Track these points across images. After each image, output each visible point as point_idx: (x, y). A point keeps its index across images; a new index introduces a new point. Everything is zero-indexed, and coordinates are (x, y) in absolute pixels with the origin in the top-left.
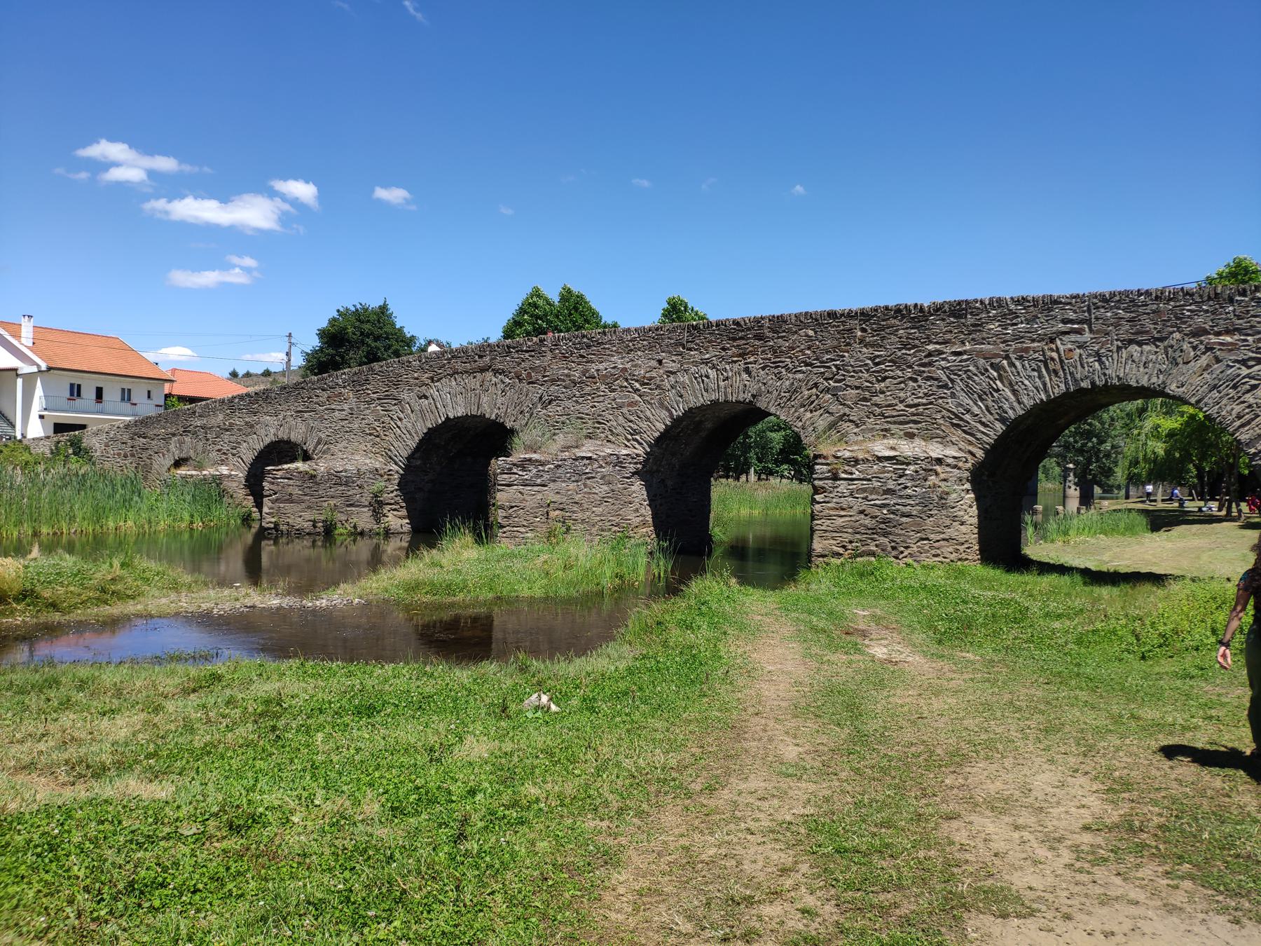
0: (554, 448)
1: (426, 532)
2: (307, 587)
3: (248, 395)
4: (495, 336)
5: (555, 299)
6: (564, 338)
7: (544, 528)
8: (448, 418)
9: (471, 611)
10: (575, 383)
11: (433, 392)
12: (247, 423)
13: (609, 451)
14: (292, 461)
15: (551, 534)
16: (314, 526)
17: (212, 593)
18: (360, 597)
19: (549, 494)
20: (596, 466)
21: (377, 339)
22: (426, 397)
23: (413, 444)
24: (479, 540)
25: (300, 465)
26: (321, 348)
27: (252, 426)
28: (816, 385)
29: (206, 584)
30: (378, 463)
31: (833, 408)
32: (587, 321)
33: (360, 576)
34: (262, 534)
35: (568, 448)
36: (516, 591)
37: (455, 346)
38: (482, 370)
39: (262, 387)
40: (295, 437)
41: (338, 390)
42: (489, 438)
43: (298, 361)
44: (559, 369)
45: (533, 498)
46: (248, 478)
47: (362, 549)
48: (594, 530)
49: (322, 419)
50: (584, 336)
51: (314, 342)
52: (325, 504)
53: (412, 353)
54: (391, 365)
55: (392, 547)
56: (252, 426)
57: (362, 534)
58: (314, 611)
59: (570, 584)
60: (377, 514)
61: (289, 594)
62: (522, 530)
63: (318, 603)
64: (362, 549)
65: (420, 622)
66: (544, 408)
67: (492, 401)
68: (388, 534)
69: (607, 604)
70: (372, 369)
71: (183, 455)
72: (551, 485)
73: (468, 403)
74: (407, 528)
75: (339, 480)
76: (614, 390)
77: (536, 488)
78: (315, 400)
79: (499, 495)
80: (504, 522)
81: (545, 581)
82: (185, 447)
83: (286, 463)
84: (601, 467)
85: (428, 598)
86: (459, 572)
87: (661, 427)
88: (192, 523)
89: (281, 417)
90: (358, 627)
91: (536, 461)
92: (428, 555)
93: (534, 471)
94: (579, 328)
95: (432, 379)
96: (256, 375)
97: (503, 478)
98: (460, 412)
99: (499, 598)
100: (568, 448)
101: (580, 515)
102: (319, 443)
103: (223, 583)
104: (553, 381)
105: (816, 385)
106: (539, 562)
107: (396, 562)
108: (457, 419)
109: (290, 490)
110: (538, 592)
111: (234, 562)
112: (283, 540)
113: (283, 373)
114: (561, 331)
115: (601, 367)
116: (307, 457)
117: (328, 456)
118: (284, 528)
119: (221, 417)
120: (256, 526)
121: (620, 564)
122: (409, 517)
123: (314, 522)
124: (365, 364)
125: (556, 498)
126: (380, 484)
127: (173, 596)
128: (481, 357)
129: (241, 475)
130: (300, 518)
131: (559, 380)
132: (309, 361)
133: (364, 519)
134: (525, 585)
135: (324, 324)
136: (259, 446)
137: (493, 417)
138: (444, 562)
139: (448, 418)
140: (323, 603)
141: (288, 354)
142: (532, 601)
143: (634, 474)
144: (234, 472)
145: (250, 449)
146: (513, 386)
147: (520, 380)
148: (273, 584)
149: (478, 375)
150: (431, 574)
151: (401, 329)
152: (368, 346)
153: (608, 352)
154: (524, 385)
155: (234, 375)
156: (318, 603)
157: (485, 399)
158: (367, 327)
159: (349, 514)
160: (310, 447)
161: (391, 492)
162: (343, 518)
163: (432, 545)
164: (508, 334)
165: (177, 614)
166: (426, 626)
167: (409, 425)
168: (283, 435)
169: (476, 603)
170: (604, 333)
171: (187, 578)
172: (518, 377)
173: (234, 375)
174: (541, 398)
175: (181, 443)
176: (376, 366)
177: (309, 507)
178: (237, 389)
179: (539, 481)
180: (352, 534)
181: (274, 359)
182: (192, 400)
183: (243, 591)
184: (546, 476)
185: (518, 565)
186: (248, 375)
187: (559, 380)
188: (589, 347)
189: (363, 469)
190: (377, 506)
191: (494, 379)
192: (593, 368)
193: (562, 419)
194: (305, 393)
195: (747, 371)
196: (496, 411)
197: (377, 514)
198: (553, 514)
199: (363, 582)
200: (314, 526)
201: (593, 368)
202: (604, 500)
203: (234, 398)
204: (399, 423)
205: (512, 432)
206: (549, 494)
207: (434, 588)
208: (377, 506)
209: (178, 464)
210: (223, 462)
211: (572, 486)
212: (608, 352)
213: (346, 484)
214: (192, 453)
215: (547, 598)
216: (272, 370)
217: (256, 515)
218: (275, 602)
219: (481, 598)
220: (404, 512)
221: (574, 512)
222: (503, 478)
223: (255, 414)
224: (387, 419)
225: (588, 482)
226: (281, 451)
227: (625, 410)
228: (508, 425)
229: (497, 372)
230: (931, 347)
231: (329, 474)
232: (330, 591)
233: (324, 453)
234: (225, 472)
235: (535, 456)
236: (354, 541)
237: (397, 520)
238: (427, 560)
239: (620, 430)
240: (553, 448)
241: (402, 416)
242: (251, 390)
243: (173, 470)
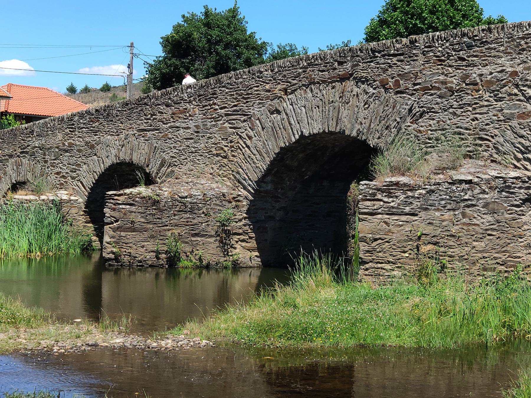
0: (425, 169)
1: (277, 267)
2: (148, 325)
3: (88, 112)
4: (357, 38)
5: (248, 33)
6: (440, 38)
7: (413, 266)
8: (302, 136)
9: (331, 360)
10: (452, 91)
11: (286, 105)
12: (87, 143)
13: (494, 173)
14: (134, 186)
15: (422, 273)
16: (158, 258)
17: (52, 329)
18: (208, 339)
19: (419, 225)
20: (477, 191)
21: (227, 46)
22: (278, 112)
23: (263, 166)
24: (338, 276)
25: (142, 190)
26: (165, 58)
27: (92, 147)
29: (45, 319)
30: (224, 187)
32: (464, 16)
33: (205, 313)
34: (103, 265)
35: (442, 170)
36: (381, 338)
37: (312, 51)
38: (343, 79)
39: (102, 104)
40: (137, 158)
41: (183, 106)
42: (350, 157)
43: (140, 73)
44: (433, 75)
45: (401, 228)
46: (88, 204)
47: (209, 282)
48: (475, 269)
49: (166, 138)
50: (464, 35)
51: (156, 52)
52: (169, 234)
53: (263, 62)
54: (239, 77)
55: (240, 283)
56: (92, 147)
57: (208, 267)
58: (157, 353)
59: (446, 332)
60: (225, 246)
61: (132, 332)
62: (388, 267)
63: (163, 343)
64: (209, 282)
65: (274, 369)
66: (415, 122)
67: (352, 114)
68: (237, 267)
69: (493, 357)
70: (219, 81)
71: (21, 179)
72: (422, 214)
73: (325, 118)
74: (257, 261)
75: (185, 206)
76: (500, 100)
77: (404, 218)
78: (158, 116)
79: (360, 226)
80: (366, 257)
81: (415, 329)
82: (22, 169)
83: (128, 187)
84: (484, 192)
85: (282, 343)
86: (316, 314)
88: (30, 251)
89: (122, 136)
90: (204, 372)
91: (405, 185)
92: (282, 293)
93: (402, 197)
94: (457, 25)
95: (285, 90)
96: (95, 91)
97: (366, 205)
98: (317, 128)
99: (362, 346)
100: (442, 170)
101: (457, 251)
102: (162, 165)
103: (64, 319)
104: (425, 89)
106: (407, 306)
107: (246, 301)
108: (313, 136)
109: (132, 217)
110: (408, 342)
111: (75, 295)
112: (125, 272)
113: (124, 89)
114: (436, 29)
115: (485, 71)
116: (149, 181)
117: (172, 180)
118: (126, 259)
119: (60, 136)
120: (96, 256)
121: (506, 310)
122: (259, 249)
123: (158, 253)
124: (213, 75)
125: (428, 230)
126: (228, 211)
127: (12, 331)
128: (340, 63)
129: (81, 200)
130: (143, 248)
131: (433, 88)
132: (152, 73)
133: (209, 250)
134: (392, 333)
135: (168, 31)
136: (100, 169)
137: (354, 134)
138: (299, 301)
139: (302, 136)
140: (168, 343)
141: (129, 66)
142: (400, 351)
143: (525, 201)
144: (75, 196)
145: (90, 171)
146: (378, 97)
147: (386, 90)
148: (115, 320)
149: (337, 84)
150: (284, 315)
151: (252, 36)
152: (218, 54)
153: (494, 53)
154: (392, 96)
155: (72, 90)
156: (163, 343)
157: (345, 113)
158: (215, 33)
159: (194, 245)
160: (152, 169)
161: (239, 220)
162: (188, 249)
163: (286, 281)
164: (372, 35)
165: (16, 351)
166: (280, 374)
167: (260, 144)
168: (125, 156)
169: (336, 350)
170: (490, 30)
171: (26, 312)
172: (384, 85)
173: (72, 90)
174: (410, 110)
175: (19, 165)
176: (224, 77)
177: (152, 237)
178: (75, 106)
179: (407, 209)
180: (197, 267)
181: (115, 72)
182: (30, 118)
183: (84, 327)
184: (416, 204)
185: (384, 309)
186: (86, 90)
187: (433, 88)
188: (470, 47)
189: (210, 193)
190: (225, 236)
191: (356, 89)
192: (474, 73)
193: (436, 134)
194: (148, 110)
196: (358, 126)
197: (225, 246)
198: (424, 249)
199: (211, 322)
200: (158, 258)
201: (474, 73)
202: (487, 233)
203: (73, 115)
204: (248, 142)
205: (376, 151)
206: (419, 225)
207: (289, 332)
208: (225, 236)
209: (15, 187)
210: (62, 186)
211: (448, 215)
212: (494, 53)
213: (191, 212)
214: (29, 177)
215: (419, 349)
216: (112, 84)
217: (96, 244)
218: (118, 341)
219: (342, 345)
220: (253, 244)
221: (450, 247)
222: (366, 205)
223: (95, 133)
224: (236, 138)
225: (467, 210)
226: (122, 174)
227: (514, 123)
228: (372, 143)
229: (359, 81)
231: (173, 199)
232: (175, 331)
233: (168, 176)
234: (65, 197)
235: (403, 180)
236: (200, 275)
237: (245, 252)
238: (279, 298)
239: (508, 147)
240: (425, 170)
241: (251, 133)
242: (91, 107)
243: (10, 194)
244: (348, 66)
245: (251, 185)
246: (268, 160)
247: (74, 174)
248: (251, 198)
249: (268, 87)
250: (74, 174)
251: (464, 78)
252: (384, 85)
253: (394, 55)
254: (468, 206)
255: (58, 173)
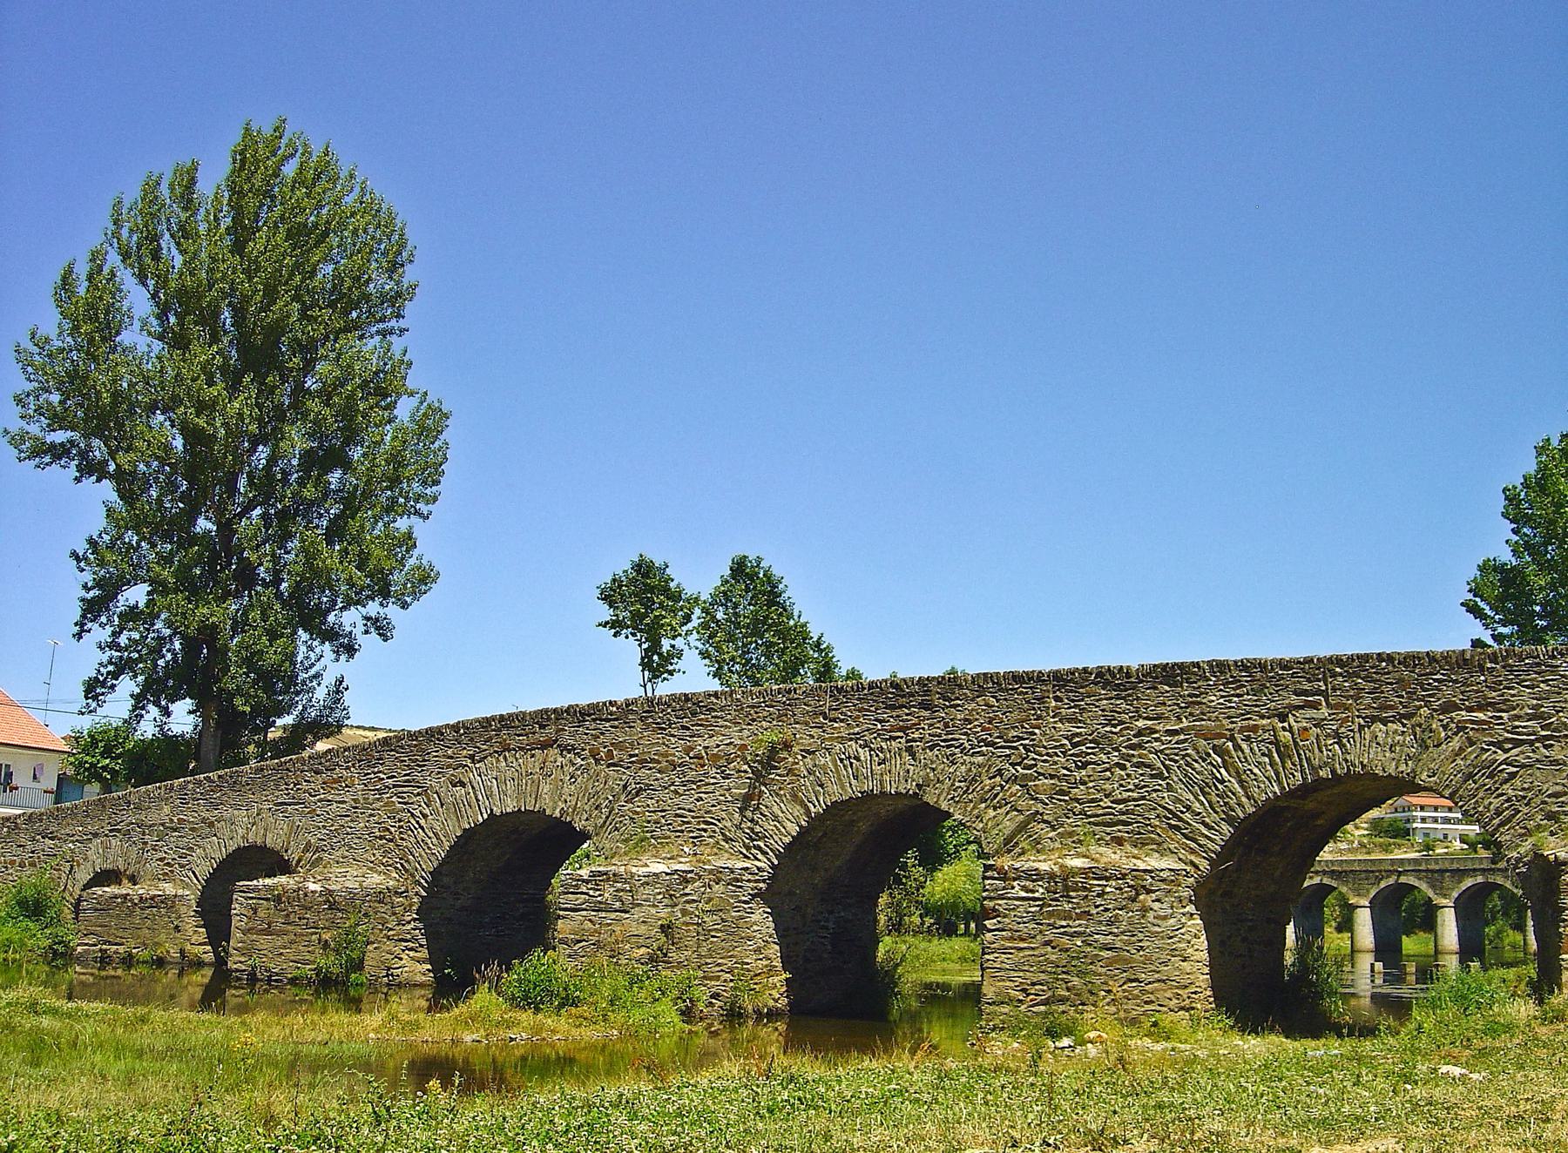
1: (449, 987)
12: (204, 820)
22: (463, 785)
27: (211, 825)
28: (1000, 772)
31: (1022, 804)
38: (545, 746)
56: (211, 825)
73: (520, 794)
76: (727, 777)
77: (613, 915)
87: (794, 829)
105: (1000, 772)
115: (711, 743)
128: (542, 727)
129: (191, 895)
136: (220, 855)
137: (557, 814)
144: (187, 892)
145: (206, 857)
147: (597, 761)
157: (545, 788)
160: (293, 855)
168: (254, 837)
172: (594, 754)
174: (625, 787)
188: (694, 714)
191: (560, 759)
192: (700, 745)
195: (910, 750)
196: (561, 805)
204: (422, 822)
210: (166, 877)
212: (721, 722)
220: (424, 954)
226: (258, 860)
229: (564, 749)
230: (1140, 723)
241: (427, 812)
244: (551, 730)
245: (423, 876)
246: (447, 845)
247: (184, 861)
248: (420, 925)
249: (450, 752)
250: (184, 861)
251: (688, 750)
252: (594, 754)
253: (608, 720)
254: (688, 902)
255: (161, 860)
